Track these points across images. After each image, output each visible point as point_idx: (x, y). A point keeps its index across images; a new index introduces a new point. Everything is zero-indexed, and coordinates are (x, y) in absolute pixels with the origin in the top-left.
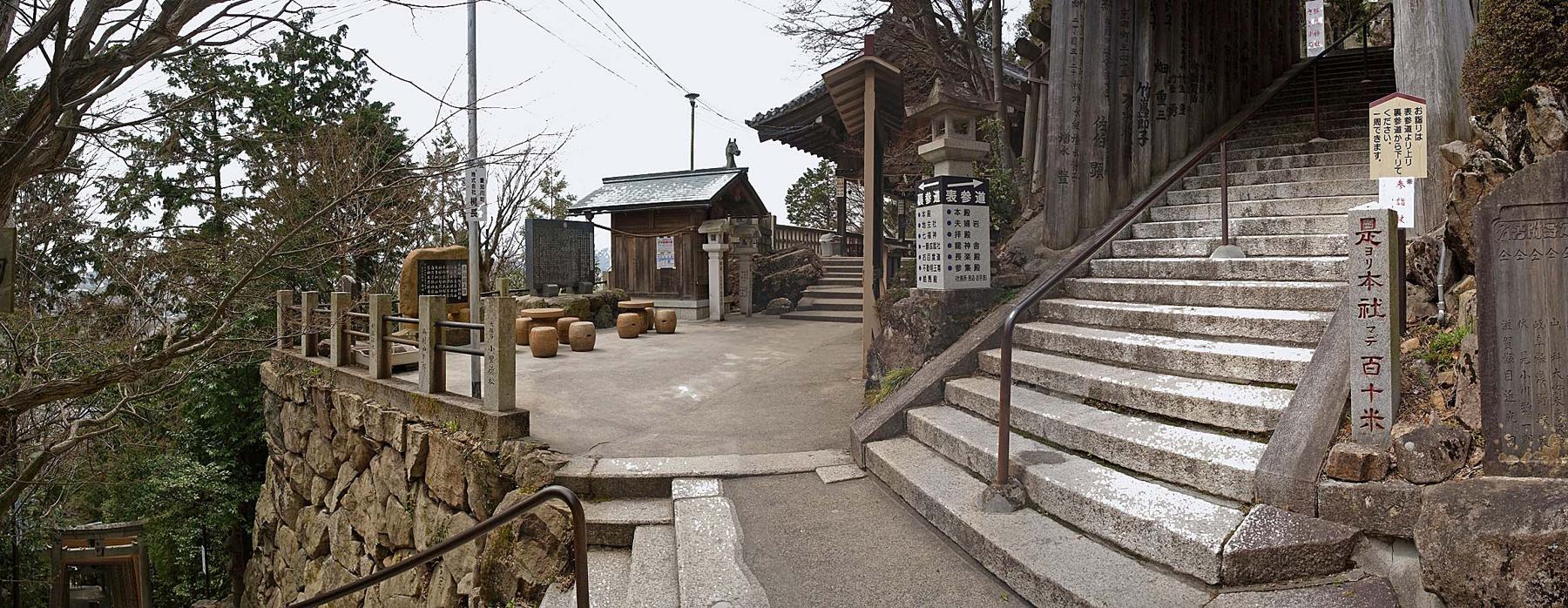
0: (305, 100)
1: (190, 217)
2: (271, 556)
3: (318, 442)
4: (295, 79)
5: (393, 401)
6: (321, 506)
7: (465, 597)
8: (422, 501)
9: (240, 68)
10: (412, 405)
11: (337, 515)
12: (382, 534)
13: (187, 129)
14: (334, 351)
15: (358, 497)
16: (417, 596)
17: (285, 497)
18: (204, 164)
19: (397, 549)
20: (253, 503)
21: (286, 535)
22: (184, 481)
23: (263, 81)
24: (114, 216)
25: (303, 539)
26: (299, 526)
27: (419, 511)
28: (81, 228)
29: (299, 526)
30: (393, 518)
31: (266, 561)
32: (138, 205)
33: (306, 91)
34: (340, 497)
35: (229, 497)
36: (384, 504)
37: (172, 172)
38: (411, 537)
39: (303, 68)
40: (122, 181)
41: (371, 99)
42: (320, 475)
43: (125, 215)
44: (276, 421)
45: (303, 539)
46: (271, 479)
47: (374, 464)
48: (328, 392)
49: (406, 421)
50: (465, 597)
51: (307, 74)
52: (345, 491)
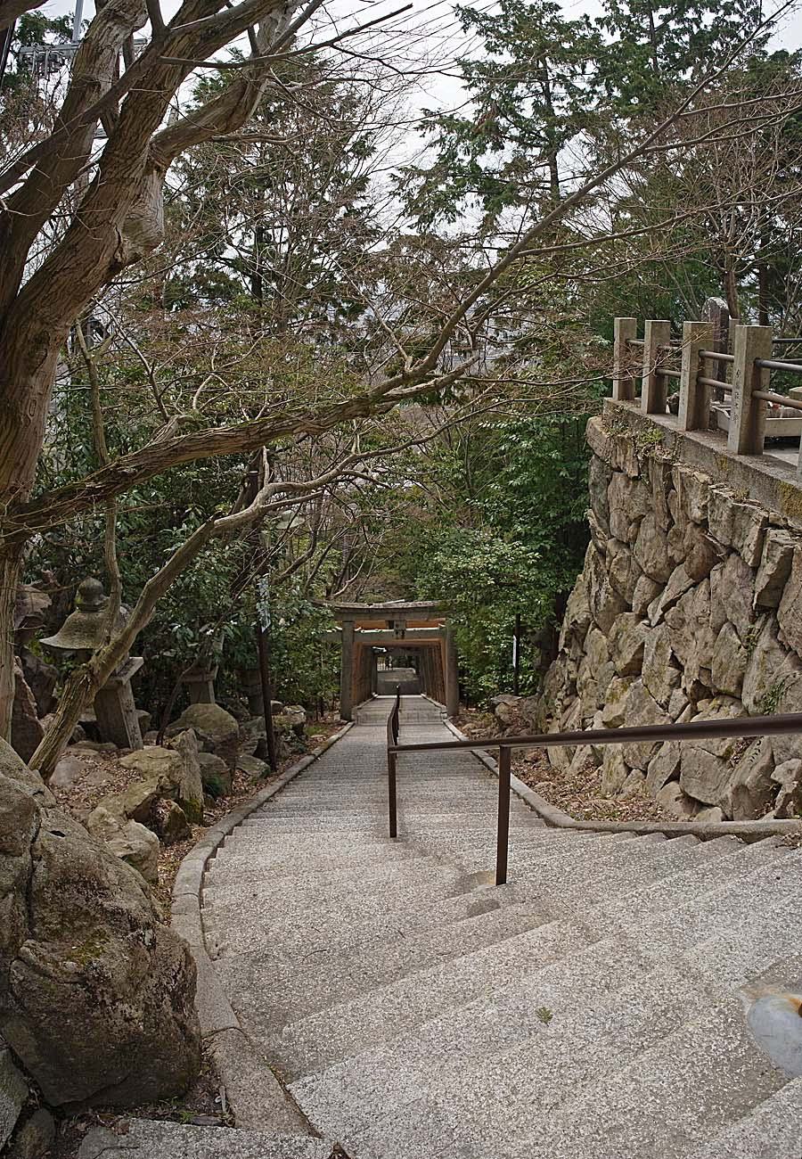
0: (673, 59)
1: (514, 218)
2: (578, 662)
3: (651, 532)
4: (656, 34)
5: (754, 491)
6: (643, 615)
7: (779, 786)
8: (765, 641)
9: (578, 25)
10: (781, 501)
11: (658, 631)
12: (705, 669)
13: (508, 107)
14: (683, 409)
15: (689, 614)
16: (724, 759)
17: (603, 595)
18: (536, 151)
19: (719, 693)
20: (566, 594)
21: (597, 640)
22: (478, 561)
23: (610, 38)
24: (415, 219)
25: (614, 651)
26: (612, 634)
27: (757, 655)
28: (373, 234)
29: (612, 634)
30: (723, 652)
31: (571, 666)
32: (445, 205)
33: (671, 47)
34: (666, 609)
35: (538, 585)
36: (717, 631)
37: (490, 161)
38: (740, 685)
39: (666, 19)
40: (428, 174)
41: (771, 48)
42: (648, 576)
43: (429, 219)
44: (601, 497)
45: (614, 651)
46: (590, 569)
47: (715, 575)
48: (668, 466)
49: (767, 523)
50: (779, 786)
51: (672, 25)
52: (672, 603)
